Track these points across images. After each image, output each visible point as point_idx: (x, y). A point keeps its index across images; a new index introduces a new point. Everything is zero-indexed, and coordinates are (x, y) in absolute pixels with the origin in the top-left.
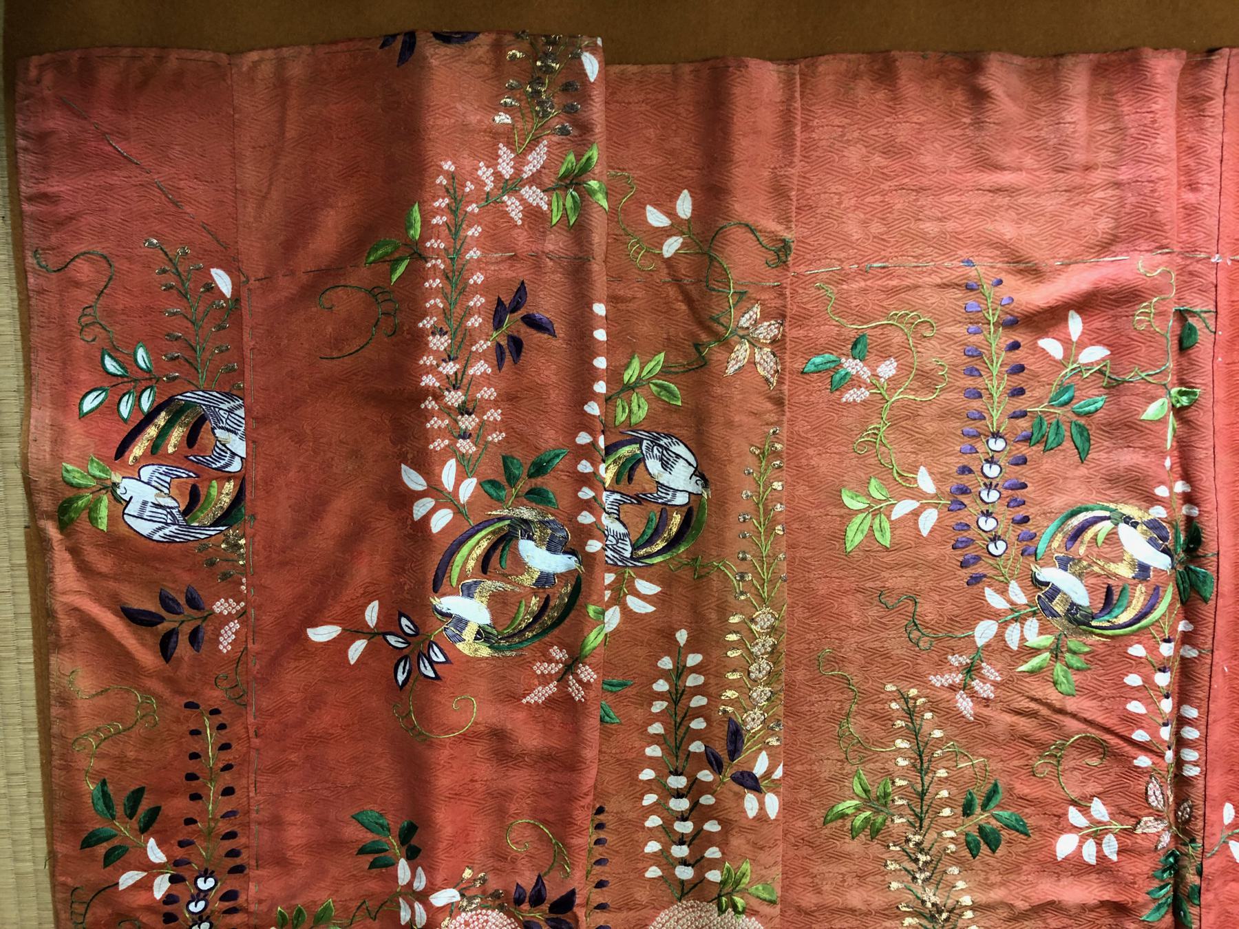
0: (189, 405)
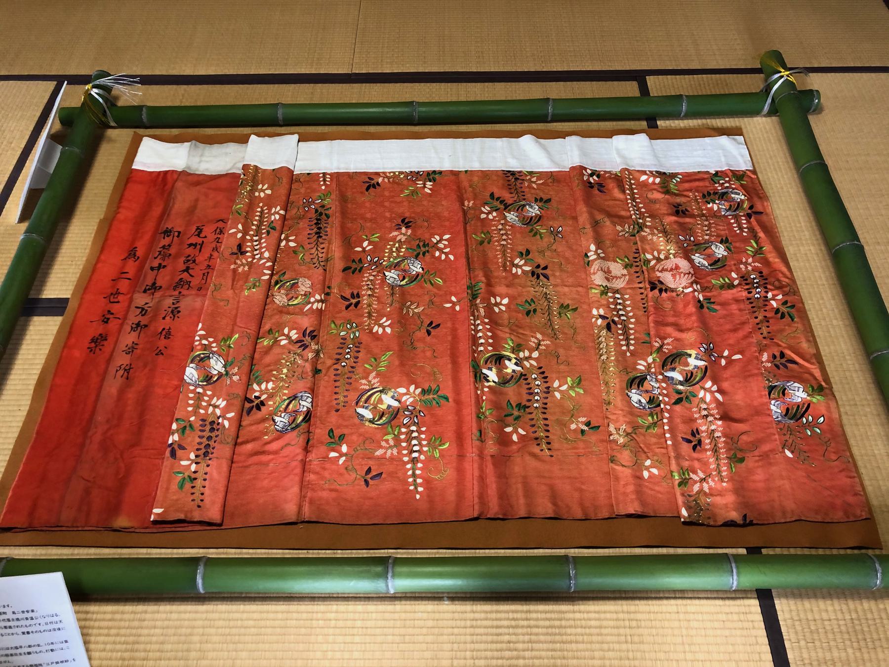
0: (791, 419)
